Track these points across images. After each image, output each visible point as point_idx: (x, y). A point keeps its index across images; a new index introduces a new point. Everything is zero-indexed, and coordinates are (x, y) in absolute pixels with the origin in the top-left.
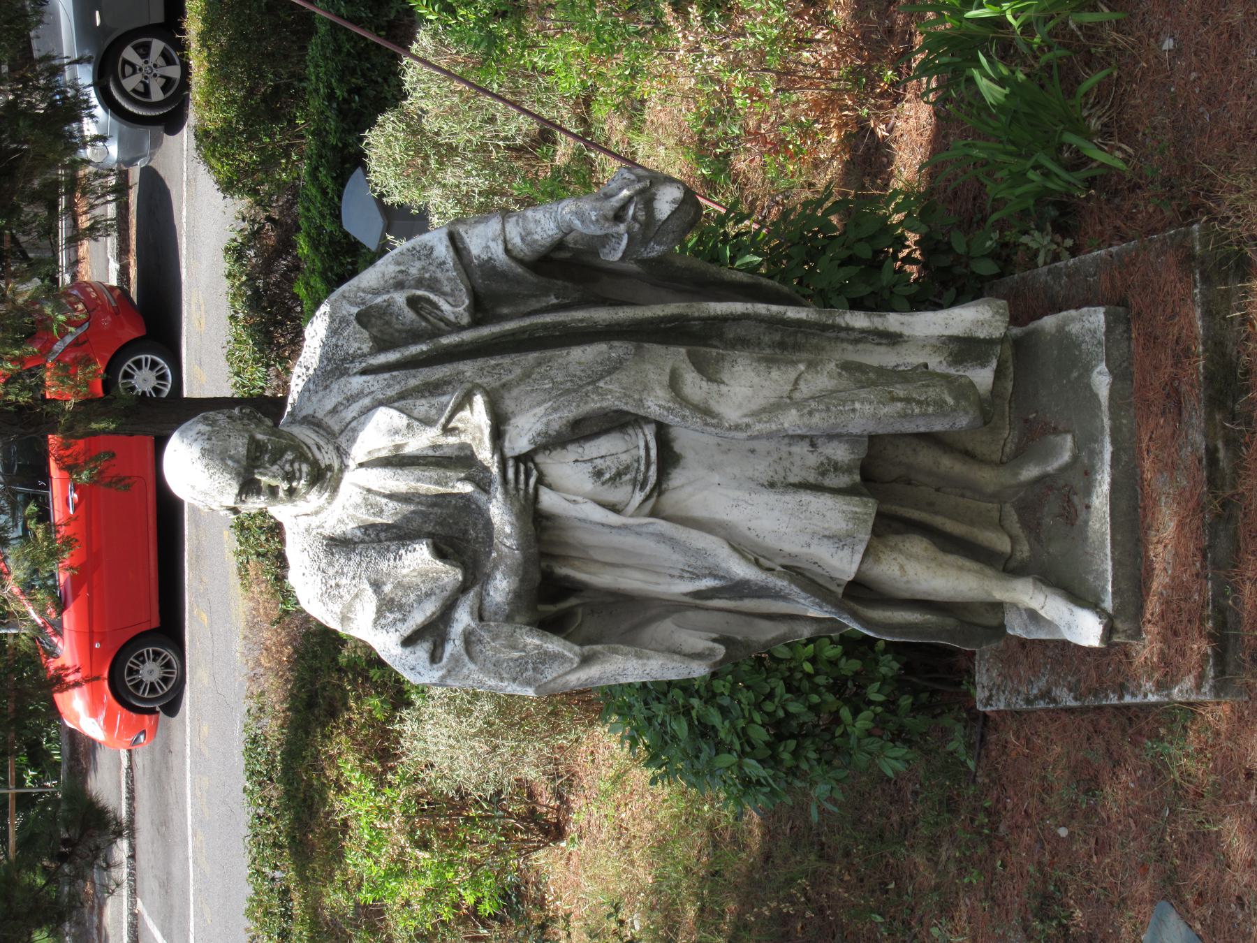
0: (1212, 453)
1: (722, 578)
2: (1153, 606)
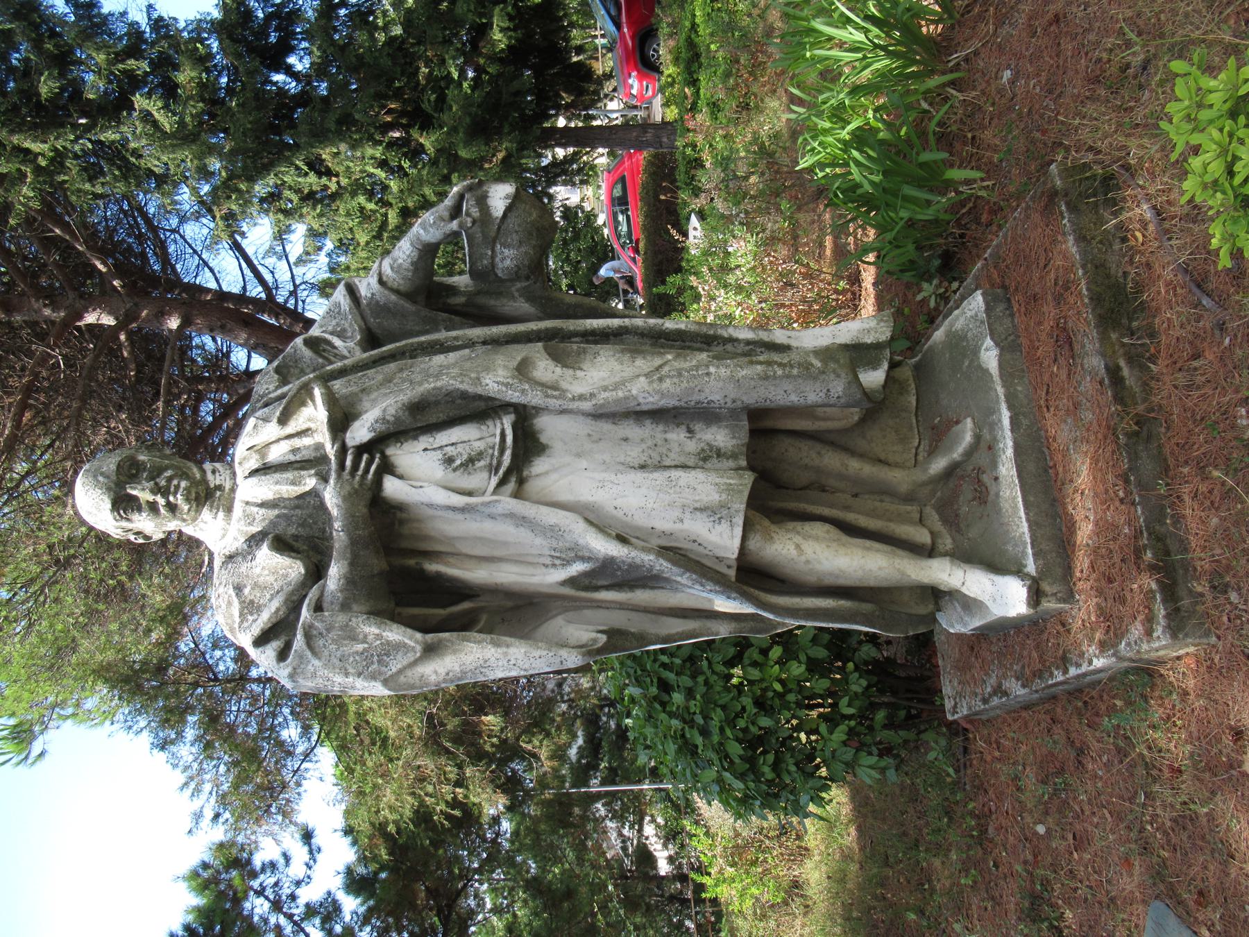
0: (1114, 373)
1: (589, 559)
2: (1082, 562)
